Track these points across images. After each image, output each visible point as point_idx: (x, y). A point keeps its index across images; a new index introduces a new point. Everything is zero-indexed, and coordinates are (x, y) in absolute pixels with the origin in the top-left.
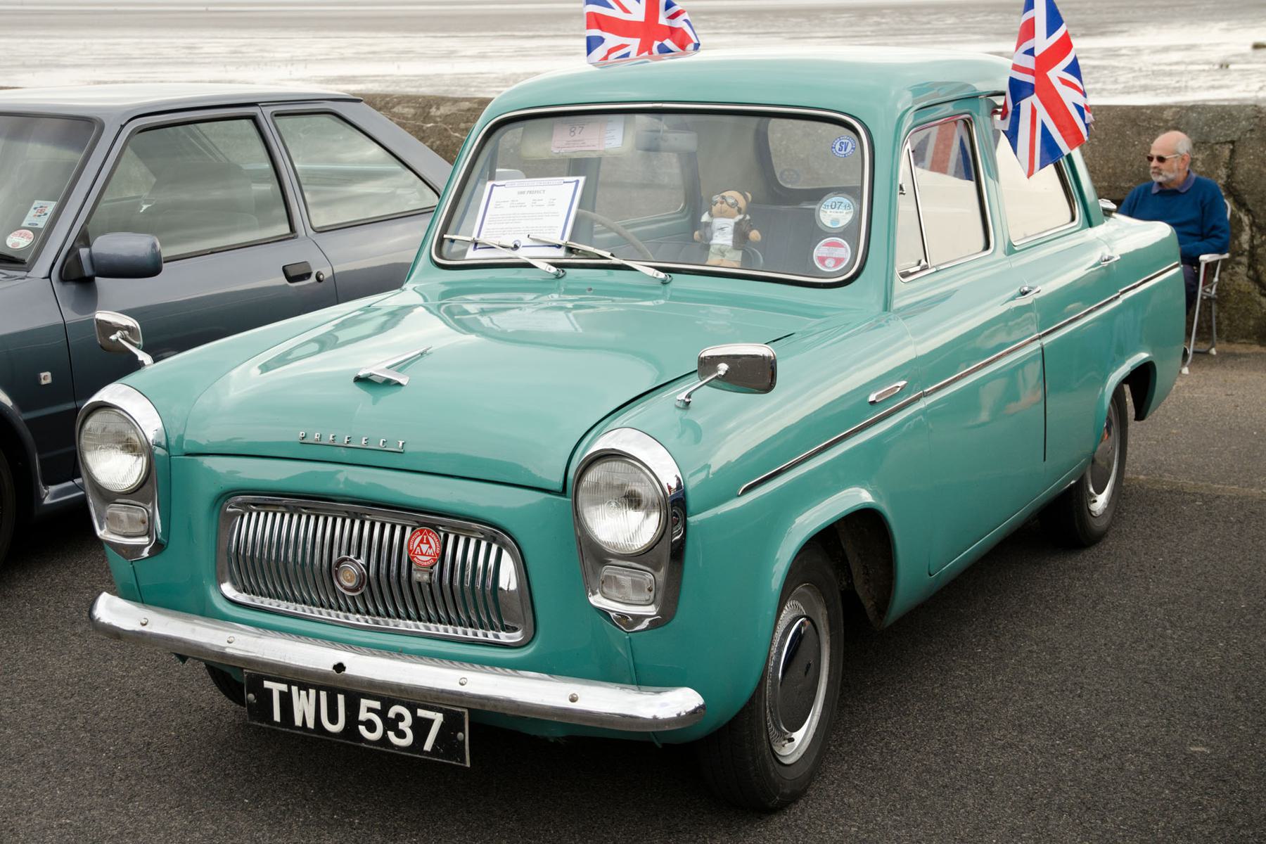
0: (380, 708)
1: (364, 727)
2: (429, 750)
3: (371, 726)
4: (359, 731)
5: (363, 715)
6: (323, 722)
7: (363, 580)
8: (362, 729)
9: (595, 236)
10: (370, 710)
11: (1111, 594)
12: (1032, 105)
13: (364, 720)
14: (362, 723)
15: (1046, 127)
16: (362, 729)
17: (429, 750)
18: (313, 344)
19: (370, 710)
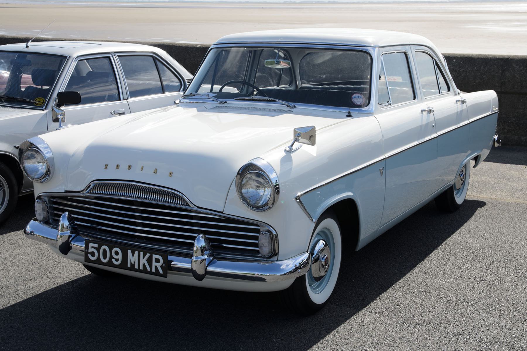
0: (97, 247)
1: (90, 255)
2: (168, 259)
3: (93, 254)
4: (88, 256)
5: (90, 250)
6: (90, 258)
7: (242, 75)
8: (90, 256)
9: (242, 84)
10: (93, 247)
11: (310, 326)
12: (143, 259)
13: (91, 252)
14: (90, 253)
15: (143, 256)
16: (90, 256)
17: (168, 259)
18: (359, 104)
19: (93, 247)
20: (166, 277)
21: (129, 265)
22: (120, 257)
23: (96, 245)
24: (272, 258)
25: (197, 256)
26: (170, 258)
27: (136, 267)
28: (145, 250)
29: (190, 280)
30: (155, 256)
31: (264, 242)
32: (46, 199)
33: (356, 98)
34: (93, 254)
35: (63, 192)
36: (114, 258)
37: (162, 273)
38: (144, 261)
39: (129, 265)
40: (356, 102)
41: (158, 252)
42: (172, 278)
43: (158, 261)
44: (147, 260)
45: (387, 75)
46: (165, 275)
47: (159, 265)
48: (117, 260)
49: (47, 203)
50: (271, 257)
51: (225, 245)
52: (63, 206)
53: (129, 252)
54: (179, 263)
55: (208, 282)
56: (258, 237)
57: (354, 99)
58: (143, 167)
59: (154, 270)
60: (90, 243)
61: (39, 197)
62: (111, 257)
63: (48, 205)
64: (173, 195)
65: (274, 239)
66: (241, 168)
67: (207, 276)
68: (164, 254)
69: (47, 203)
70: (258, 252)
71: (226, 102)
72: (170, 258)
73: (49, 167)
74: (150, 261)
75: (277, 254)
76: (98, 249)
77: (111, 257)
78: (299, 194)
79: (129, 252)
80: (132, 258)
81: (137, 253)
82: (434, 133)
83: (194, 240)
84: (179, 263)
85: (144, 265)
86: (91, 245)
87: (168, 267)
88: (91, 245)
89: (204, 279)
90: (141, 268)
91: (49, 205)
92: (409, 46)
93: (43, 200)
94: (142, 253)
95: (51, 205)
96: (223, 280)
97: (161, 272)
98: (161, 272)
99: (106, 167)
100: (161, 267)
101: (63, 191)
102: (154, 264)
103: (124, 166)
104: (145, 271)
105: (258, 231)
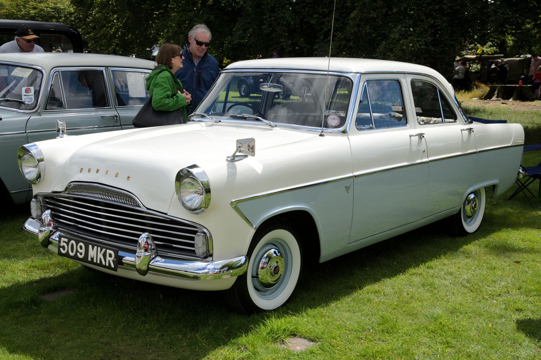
5: (62, 244)
8: (61, 249)
10: (64, 242)
16: (61, 249)
19: (64, 242)
20: (117, 271)
21: (89, 259)
22: (83, 251)
23: (66, 240)
24: (208, 258)
25: (141, 253)
26: (121, 253)
27: (95, 261)
28: (102, 246)
29: (135, 276)
30: (109, 251)
31: (199, 241)
32: (41, 199)
33: (332, 119)
34: (64, 248)
35: (50, 192)
36: (79, 252)
37: (113, 267)
38: (100, 256)
39: (89, 259)
40: (331, 123)
41: (111, 247)
42: (121, 272)
43: (110, 255)
44: (103, 255)
45: (8, 85)
46: (115, 269)
47: (111, 259)
48: (81, 254)
49: (41, 203)
50: (206, 257)
51: (174, 245)
52: (74, 209)
53: (90, 246)
54: (128, 258)
55: (150, 278)
56: (194, 238)
57: (329, 120)
58: (107, 171)
59: (107, 265)
60: (62, 238)
61: (36, 197)
62: (77, 251)
63: (42, 204)
64: (128, 197)
65: (208, 239)
66: (479, 210)
67: (149, 271)
68: (116, 250)
69: (41, 203)
70: (194, 251)
71: (220, 121)
72: (121, 253)
73: (40, 171)
74: (104, 255)
75: (211, 255)
76: (68, 243)
77: (77, 251)
78: (233, 201)
79: (90, 246)
80: (93, 253)
81: (95, 247)
82: (425, 158)
83: (139, 237)
84: (128, 258)
85: (100, 259)
86: (63, 239)
87: (119, 261)
88: (63, 239)
89: (147, 274)
90: (98, 262)
91: (43, 204)
92: (404, 75)
93: (39, 200)
94: (99, 248)
95: (45, 205)
96: (163, 276)
97: (113, 266)
98: (113, 266)
99: (81, 170)
100: (113, 261)
101: (50, 192)
102: (108, 258)
103: (94, 170)
104: (101, 265)
105: (195, 232)
